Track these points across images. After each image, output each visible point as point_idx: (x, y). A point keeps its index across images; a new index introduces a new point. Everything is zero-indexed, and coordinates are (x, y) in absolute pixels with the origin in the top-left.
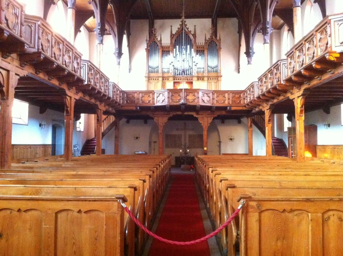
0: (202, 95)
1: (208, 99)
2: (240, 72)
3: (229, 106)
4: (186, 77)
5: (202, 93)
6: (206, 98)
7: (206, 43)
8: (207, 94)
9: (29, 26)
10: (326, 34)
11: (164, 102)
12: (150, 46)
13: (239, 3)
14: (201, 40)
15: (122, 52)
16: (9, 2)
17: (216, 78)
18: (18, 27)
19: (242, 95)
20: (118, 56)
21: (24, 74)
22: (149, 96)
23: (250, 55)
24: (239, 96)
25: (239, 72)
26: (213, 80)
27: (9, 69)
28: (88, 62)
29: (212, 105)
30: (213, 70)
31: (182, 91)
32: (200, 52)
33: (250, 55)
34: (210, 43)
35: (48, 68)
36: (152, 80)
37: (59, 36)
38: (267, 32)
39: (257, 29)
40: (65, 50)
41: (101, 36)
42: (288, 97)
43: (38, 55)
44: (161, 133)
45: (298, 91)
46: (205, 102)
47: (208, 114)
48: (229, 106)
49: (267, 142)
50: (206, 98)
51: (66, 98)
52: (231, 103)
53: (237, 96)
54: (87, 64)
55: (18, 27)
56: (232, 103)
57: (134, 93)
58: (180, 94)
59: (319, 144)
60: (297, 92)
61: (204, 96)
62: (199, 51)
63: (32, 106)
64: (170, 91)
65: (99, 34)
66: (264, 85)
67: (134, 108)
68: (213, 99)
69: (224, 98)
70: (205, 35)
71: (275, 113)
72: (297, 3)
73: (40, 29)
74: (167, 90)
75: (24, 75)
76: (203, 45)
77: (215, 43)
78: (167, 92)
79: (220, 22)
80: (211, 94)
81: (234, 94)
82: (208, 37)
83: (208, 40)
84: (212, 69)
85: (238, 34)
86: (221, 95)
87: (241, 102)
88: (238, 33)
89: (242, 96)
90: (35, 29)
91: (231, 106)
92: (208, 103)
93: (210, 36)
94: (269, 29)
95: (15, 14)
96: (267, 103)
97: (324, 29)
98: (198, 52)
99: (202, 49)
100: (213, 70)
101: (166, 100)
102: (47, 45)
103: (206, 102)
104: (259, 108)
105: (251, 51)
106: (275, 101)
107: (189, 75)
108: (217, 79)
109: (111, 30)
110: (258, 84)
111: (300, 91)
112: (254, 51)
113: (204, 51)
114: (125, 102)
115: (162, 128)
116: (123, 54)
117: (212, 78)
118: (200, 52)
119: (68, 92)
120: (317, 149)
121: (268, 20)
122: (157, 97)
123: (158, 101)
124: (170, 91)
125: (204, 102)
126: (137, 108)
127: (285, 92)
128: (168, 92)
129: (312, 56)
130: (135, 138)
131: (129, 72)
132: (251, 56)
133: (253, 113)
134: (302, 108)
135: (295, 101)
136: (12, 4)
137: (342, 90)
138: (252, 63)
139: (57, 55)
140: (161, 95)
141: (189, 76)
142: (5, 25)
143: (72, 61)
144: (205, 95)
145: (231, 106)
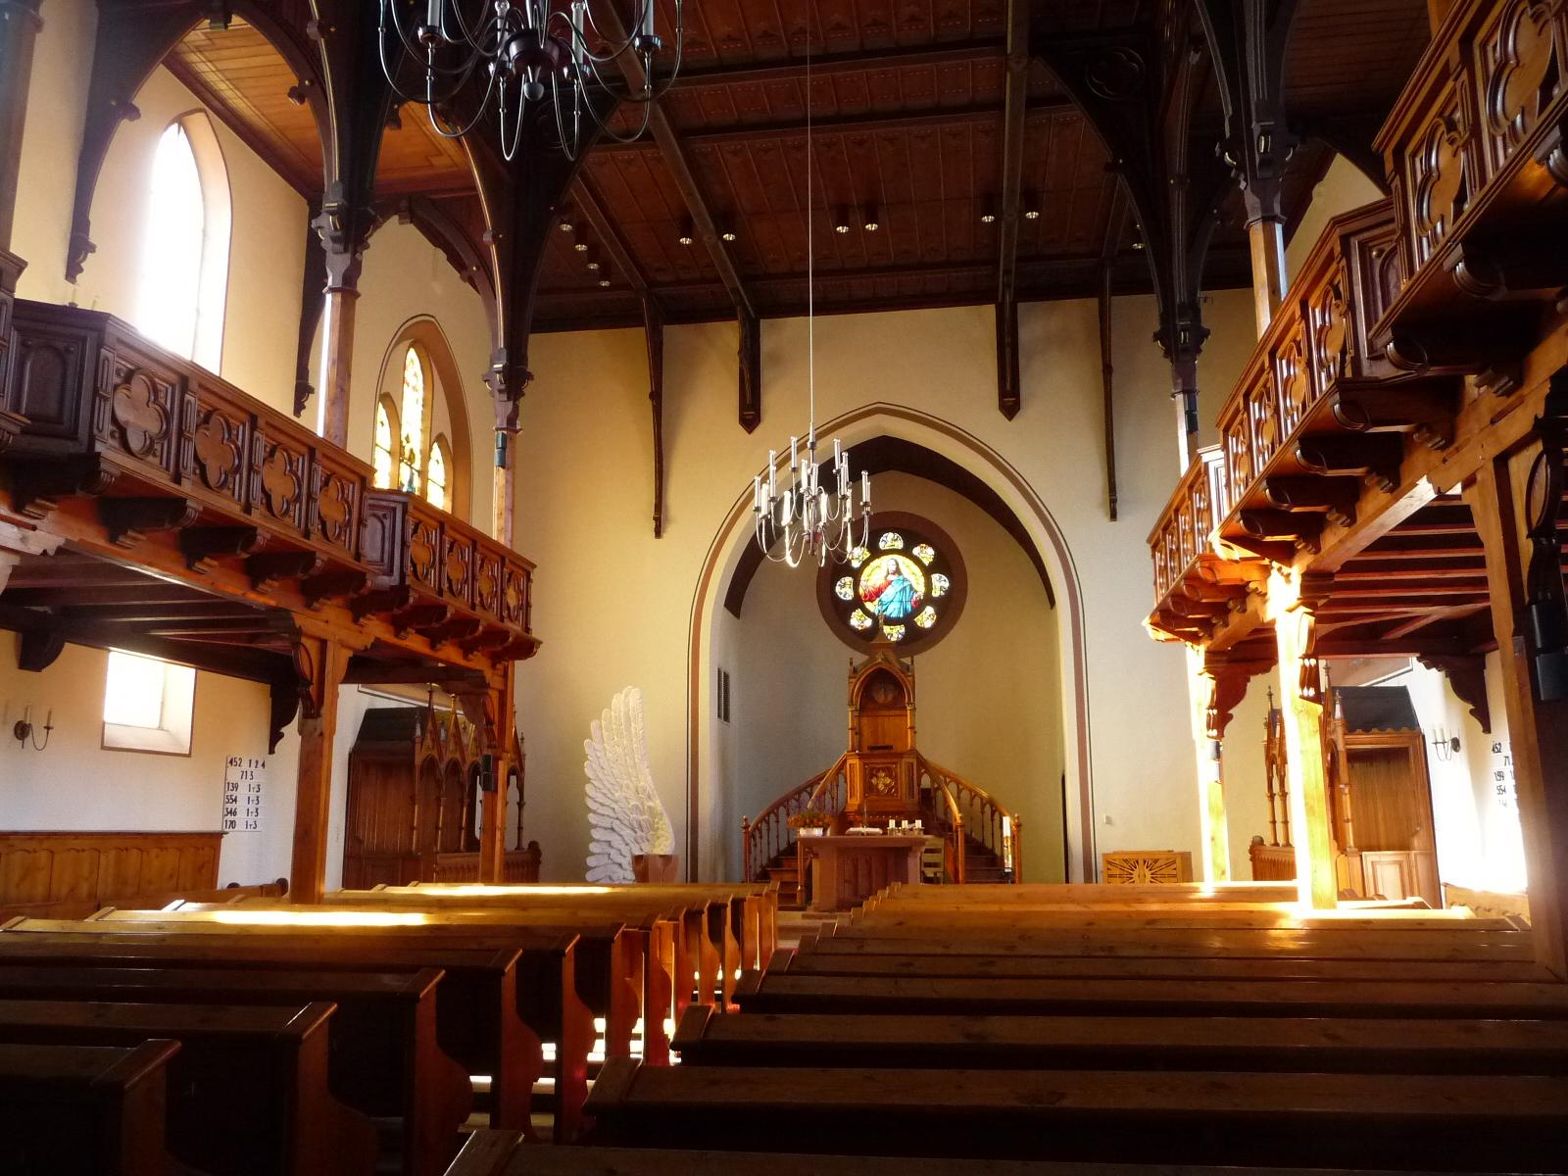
9: (56, 350)
16: (210, 409)
18: (350, 534)
27: (324, 636)
37: (173, 366)
40: (448, 546)
41: (509, 399)
51: (487, 694)
55: (350, 534)
63: (204, 674)
65: (500, 391)
73: (258, 439)
90: (394, 526)
102: (340, 518)
119: (303, 620)
131: (658, 533)
139: (458, 580)
143: (502, 590)
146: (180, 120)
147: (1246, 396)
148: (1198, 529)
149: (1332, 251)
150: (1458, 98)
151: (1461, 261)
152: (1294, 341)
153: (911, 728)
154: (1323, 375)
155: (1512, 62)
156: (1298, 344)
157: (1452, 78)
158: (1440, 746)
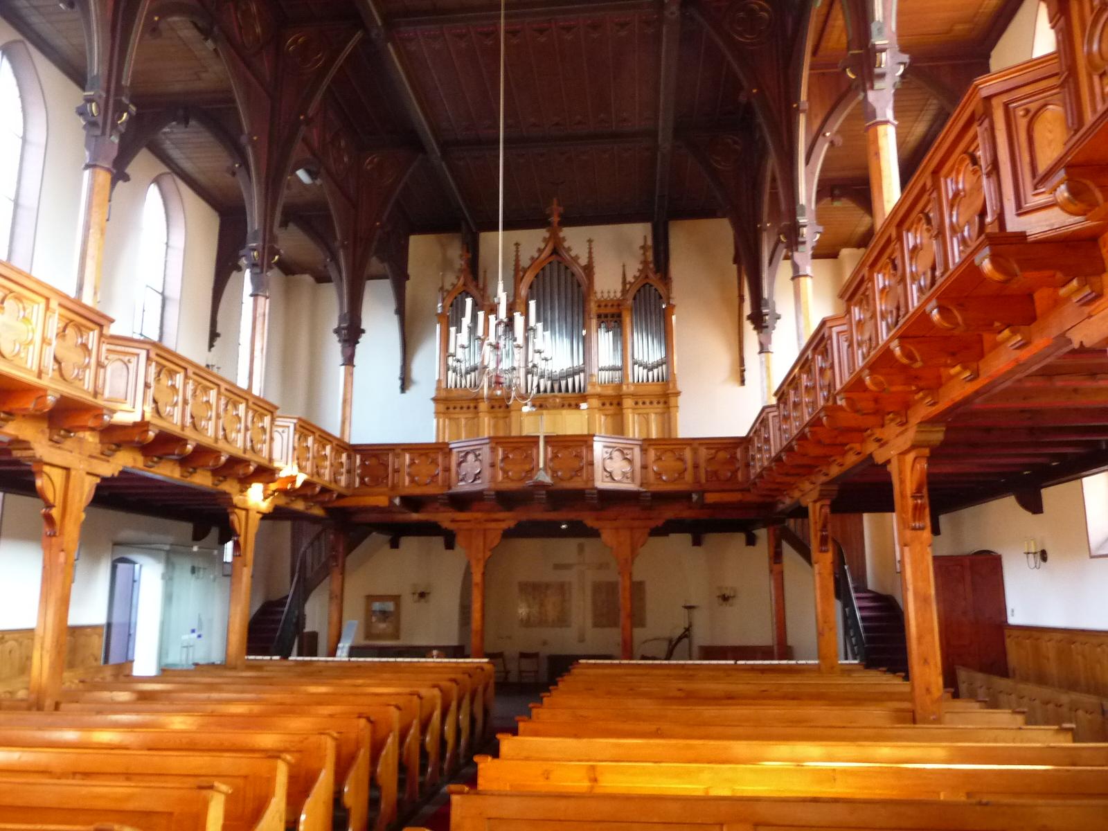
2: (746, 382)
3: (696, 492)
4: (563, 398)
7: (624, 292)
10: (975, 172)
12: (451, 305)
14: (607, 283)
15: (363, 326)
17: (662, 400)
20: (346, 338)
22: (434, 462)
23: (764, 324)
24: (731, 457)
25: (743, 382)
26: (644, 406)
28: (148, 347)
32: (609, 318)
33: (764, 324)
38: (801, 239)
42: (870, 456)
45: (902, 433)
46: (616, 478)
47: (633, 519)
48: (696, 492)
49: (820, 617)
52: (703, 481)
53: (722, 455)
54: (143, 354)
56: (707, 481)
59: (1013, 620)
60: (897, 436)
61: (611, 458)
62: (606, 316)
64: (646, 444)
66: (794, 414)
67: (382, 501)
68: (644, 467)
69: (507, 468)
70: (624, 266)
71: (864, 512)
72: (879, 112)
74: (487, 441)
78: (488, 446)
79: (681, 236)
80: (637, 451)
81: (712, 448)
82: (633, 271)
83: (633, 280)
84: (649, 370)
86: (669, 454)
87: (736, 477)
91: (705, 491)
92: (625, 480)
93: (639, 270)
94: (805, 230)
96: (813, 478)
98: (603, 319)
99: (614, 310)
101: (487, 473)
104: (792, 498)
105: (765, 311)
106: (835, 471)
107: (560, 390)
108: (665, 403)
109: (331, 261)
110: (776, 413)
111: (906, 430)
112: (778, 311)
113: (620, 315)
114: (354, 482)
116: (363, 331)
117: (648, 401)
118: (609, 318)
120: (1008, 641)
121: (802, 199)
122: (459, 464)
123: (461, 477)
125: (613, 479)
126: (391, 502)
127: (859, 432)
130: (416, 596)
133: (782, 512)
134: (921, 497)
135: (893, 468)
137: (819, 4)
138: (772, 347)
140: (471, 457)
141: (574, 395)
144: (616, 454)
145: (705, 491)
146: (157, 181)
147: (815, 349)
148: (912, 271)
149: (925, 185)
150: (979, 140)
151: (1063, 183)
152: (889, 258)
153: (899, 561)
154: (915, 287)
155: (962, 194)
156: (893, 261)
157: (928, 193)
158: (1031, 556)
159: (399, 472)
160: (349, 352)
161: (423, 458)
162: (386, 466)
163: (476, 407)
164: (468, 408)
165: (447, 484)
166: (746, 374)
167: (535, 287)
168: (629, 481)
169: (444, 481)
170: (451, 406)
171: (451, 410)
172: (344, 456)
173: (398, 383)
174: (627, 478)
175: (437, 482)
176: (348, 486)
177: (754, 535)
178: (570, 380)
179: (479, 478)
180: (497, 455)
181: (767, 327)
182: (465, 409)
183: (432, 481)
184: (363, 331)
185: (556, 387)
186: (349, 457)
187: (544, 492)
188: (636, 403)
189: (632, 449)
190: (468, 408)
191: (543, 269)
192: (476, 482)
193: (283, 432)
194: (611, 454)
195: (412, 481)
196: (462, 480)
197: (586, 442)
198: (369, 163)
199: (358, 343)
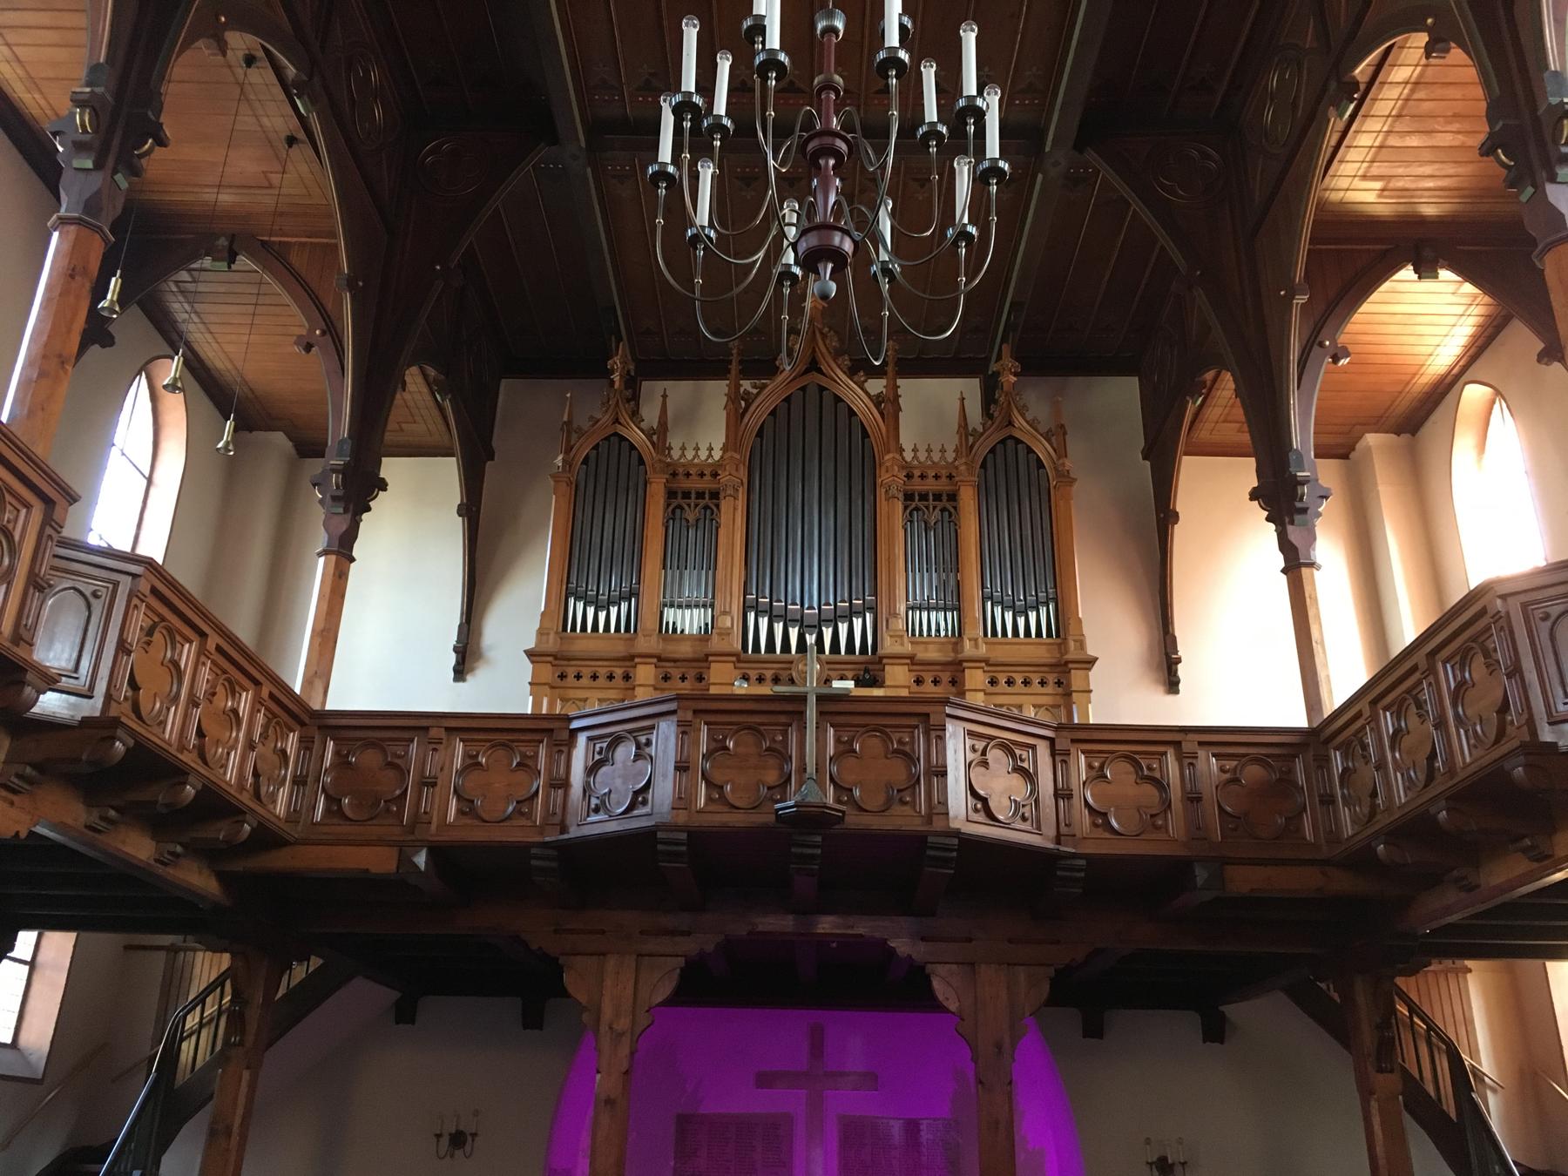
0: (971, 756)
1: (1018, 788)
5: (971, 734)
6: (1002, 786)
8: (1007, 748)
11: (646, 810)
12: (586, 461)
13: (1181, 197)
16: (156, 619)
17: (1051, 678)
19: (1299, 766)
20: (340, 493)
21: (18, 827)
22: (528, 765)
29: (1058, 842)
30: (1021, 621)
31: (802, 714)
34: (992, 451)
35: (81, 760)
36: (585, 681)
39: (1321, 345)
43: (105, 733)
44: (609, 1102)
50: (1002, 786)
53: (1253, 772)
57: (406, 735)
58: (785, 742)
61: (985, 764)
62: (923, 497)
67: (380, 861)
68: (1062, 794)
75: (17, 833)
76: (950, 460)
77: (1030, 450)
80: (1043, 750)
85: (1148, 463)
88: (1145, 458)
89: (1301, 778)
92: (1019, 825)
95: (174, 665)
97: (1408, 691)
99: (943, 486)
100: (1021, 621)
103: (1002, 810)
109: (323, 333)
115: (624, 1050)
117: (1019, 679)
124: (696, 712)
125: (990, 815)
126: (405, 860)
128: (680, 724)
129: (1366, 810)
132: (1304, 511)
136: (164, 627)
140: (625, 751)
141: (863, 658)
142: (195, 755)
144: (994, 755)
159: (434, 785)
160: (342, 525)
161: (501, 753)
162: (403, 772)
163: (627, 677)
164: (611, 677)
165: (557, 820)
166: (1182, 670)
167: (768, 433)
168: (1026, 826)
169: (548, 814)
170: (571, 672)
171: (571, 680)
172: (292, 743)
173: (452, 659)
174: (1024, 819)
175: (529, 816)
176: (293, 816)
177: (1223, 1017)
178: (843, 628)
179: (645, 802)
180: (697, 743)
181: (1304, 511)
182: (602, 681)
183: (518, 812)
184: (383, 486)
185: (811, 639)
186: (306, 744)
187: (819, 839)
188: (993, 682)
189: (1033, 747)
190: (611, 677)
191: (787, 400)
192: (636, 812)
193: (95, 595)
194: (984, 753)
195: (468, 807)
196: (597, 810)
197: (926, 716)
198: (431, 152)
199: (368, 509)
